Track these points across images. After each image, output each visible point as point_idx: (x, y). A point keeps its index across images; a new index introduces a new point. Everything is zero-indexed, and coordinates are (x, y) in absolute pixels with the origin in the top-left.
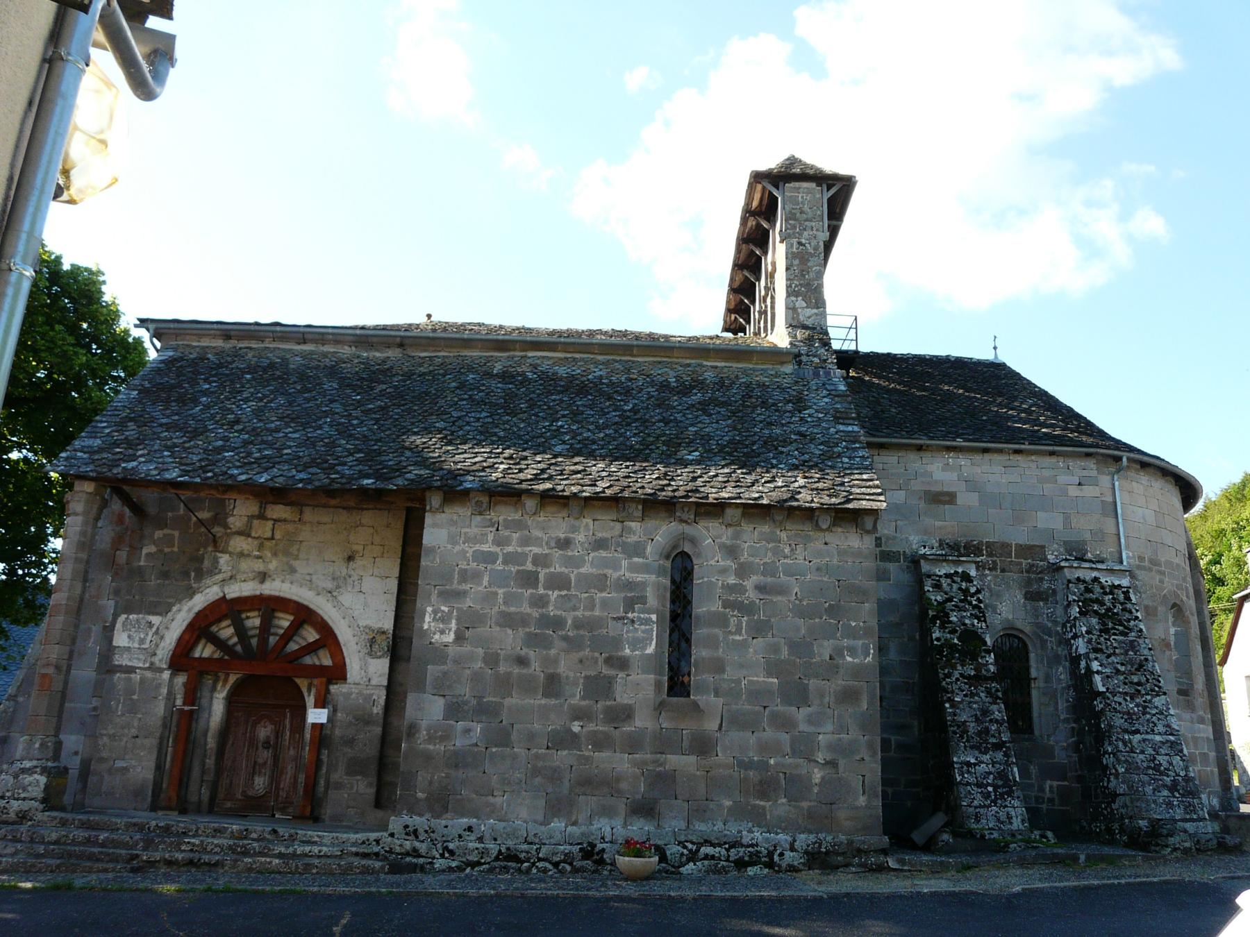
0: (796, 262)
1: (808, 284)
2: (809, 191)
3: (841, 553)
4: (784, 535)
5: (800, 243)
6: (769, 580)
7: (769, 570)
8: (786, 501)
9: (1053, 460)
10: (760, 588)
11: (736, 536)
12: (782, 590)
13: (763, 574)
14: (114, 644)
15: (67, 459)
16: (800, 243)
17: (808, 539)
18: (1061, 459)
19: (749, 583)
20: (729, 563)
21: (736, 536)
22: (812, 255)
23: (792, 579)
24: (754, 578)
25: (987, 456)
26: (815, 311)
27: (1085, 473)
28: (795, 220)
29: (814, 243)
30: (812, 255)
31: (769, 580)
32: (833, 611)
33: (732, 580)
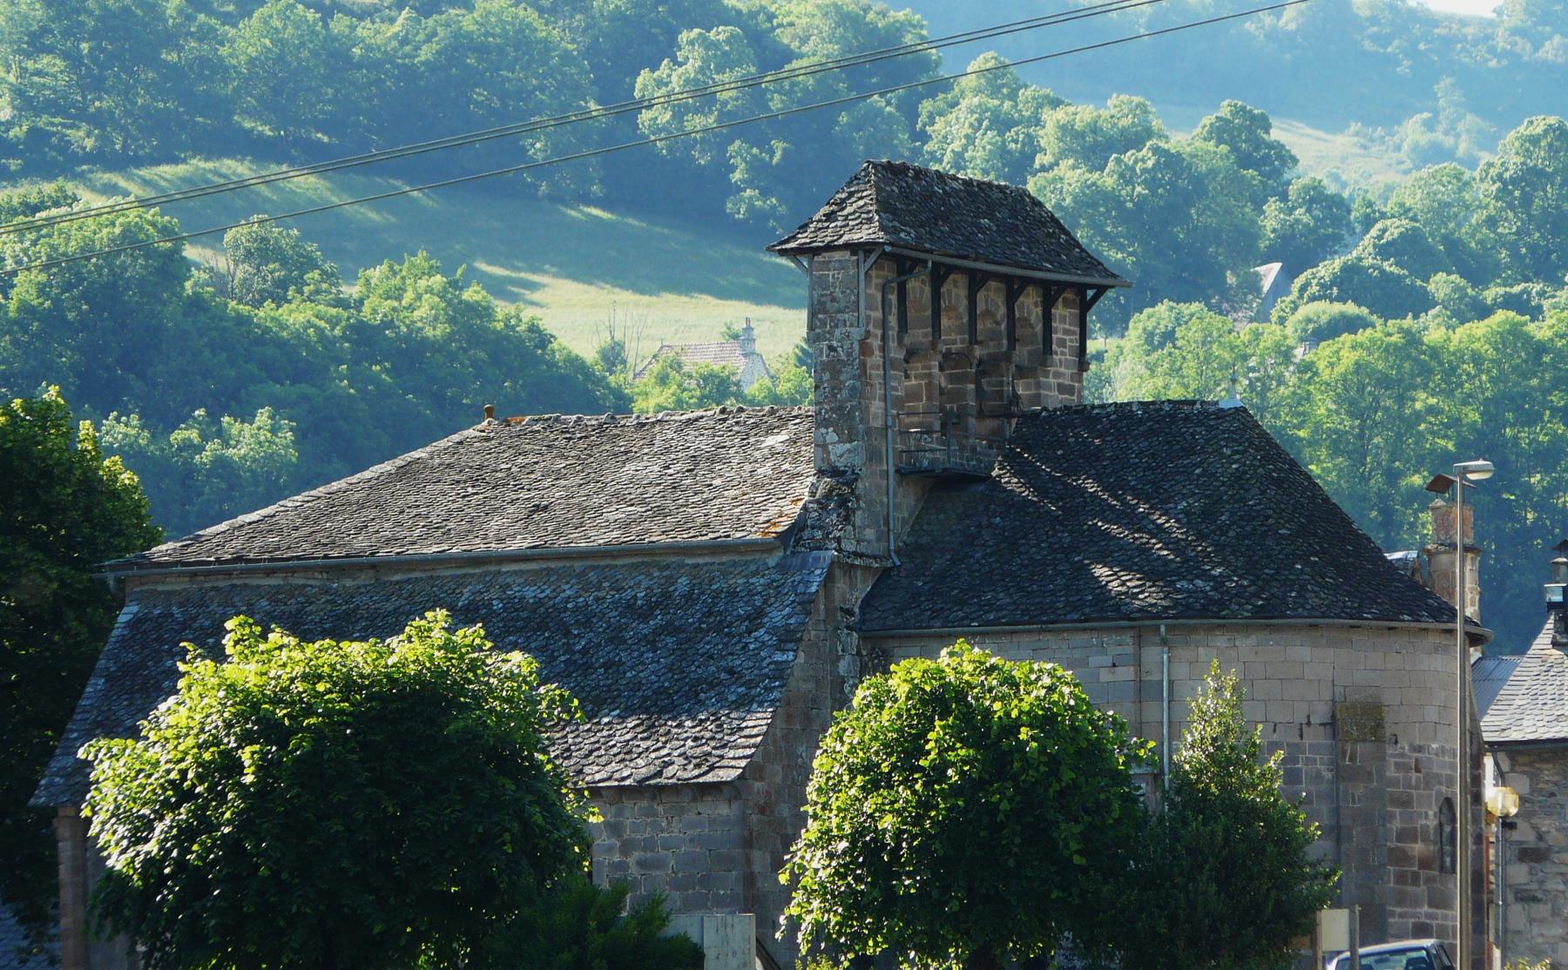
0: (826, 376)
1: (841, 408)
2: (842, 266)
3: (712, 822)
4: (660, 809)
5: (831, 348)
6: (649, 855)
7: (649, 845)
8: (648, 779)
9: (1086, 636)
10: (641, 864)
11: (619, 814)
12: (659, 864)
13: (644, 849)
14: (802, 316)
15: (47, 787)
16: (831, 348)
17: (682, 811)
18: (1095, 634)
19: (631, 860)
20: (613, 840)
21: (619, 814)
22: (845, 364)
23: (669, 853)
24: (636, 854)
25: (1016, 638)
26: (848, 446)
27: (1119, 650)
28: (825, 312)
29: (847, 345)
30: (845, 364)
31: (649, 855)
32: (706, 880)
33: (617, 858)
